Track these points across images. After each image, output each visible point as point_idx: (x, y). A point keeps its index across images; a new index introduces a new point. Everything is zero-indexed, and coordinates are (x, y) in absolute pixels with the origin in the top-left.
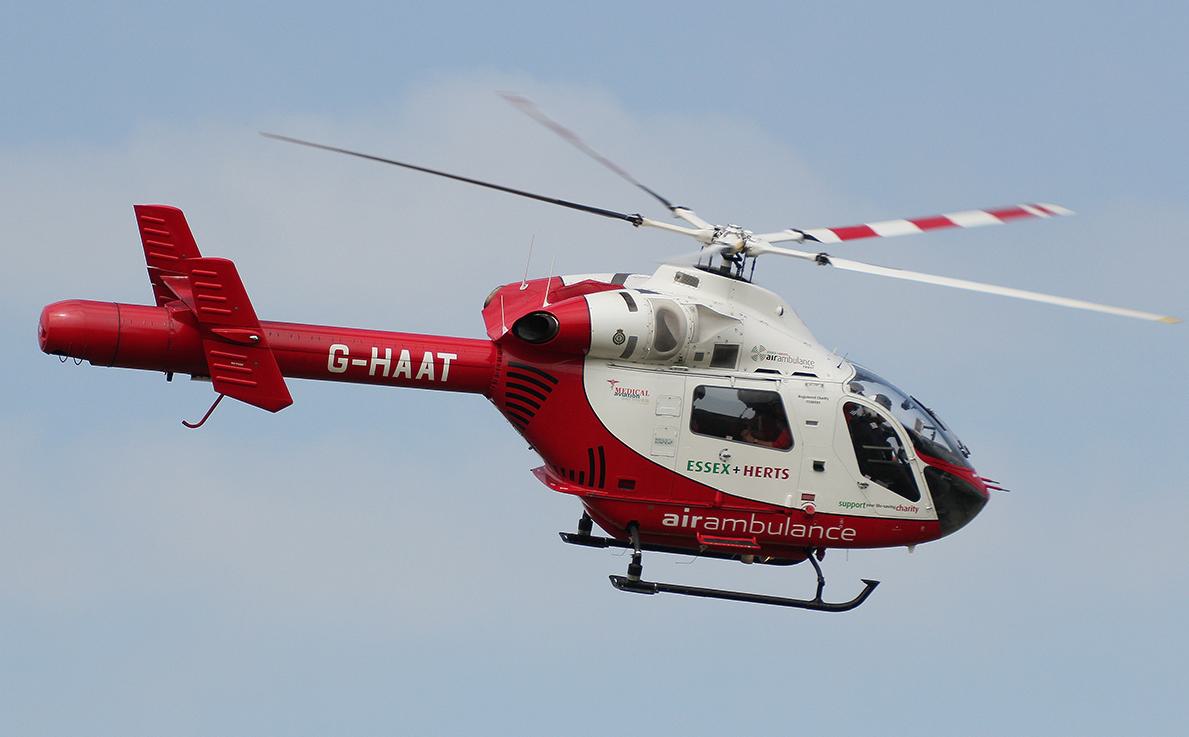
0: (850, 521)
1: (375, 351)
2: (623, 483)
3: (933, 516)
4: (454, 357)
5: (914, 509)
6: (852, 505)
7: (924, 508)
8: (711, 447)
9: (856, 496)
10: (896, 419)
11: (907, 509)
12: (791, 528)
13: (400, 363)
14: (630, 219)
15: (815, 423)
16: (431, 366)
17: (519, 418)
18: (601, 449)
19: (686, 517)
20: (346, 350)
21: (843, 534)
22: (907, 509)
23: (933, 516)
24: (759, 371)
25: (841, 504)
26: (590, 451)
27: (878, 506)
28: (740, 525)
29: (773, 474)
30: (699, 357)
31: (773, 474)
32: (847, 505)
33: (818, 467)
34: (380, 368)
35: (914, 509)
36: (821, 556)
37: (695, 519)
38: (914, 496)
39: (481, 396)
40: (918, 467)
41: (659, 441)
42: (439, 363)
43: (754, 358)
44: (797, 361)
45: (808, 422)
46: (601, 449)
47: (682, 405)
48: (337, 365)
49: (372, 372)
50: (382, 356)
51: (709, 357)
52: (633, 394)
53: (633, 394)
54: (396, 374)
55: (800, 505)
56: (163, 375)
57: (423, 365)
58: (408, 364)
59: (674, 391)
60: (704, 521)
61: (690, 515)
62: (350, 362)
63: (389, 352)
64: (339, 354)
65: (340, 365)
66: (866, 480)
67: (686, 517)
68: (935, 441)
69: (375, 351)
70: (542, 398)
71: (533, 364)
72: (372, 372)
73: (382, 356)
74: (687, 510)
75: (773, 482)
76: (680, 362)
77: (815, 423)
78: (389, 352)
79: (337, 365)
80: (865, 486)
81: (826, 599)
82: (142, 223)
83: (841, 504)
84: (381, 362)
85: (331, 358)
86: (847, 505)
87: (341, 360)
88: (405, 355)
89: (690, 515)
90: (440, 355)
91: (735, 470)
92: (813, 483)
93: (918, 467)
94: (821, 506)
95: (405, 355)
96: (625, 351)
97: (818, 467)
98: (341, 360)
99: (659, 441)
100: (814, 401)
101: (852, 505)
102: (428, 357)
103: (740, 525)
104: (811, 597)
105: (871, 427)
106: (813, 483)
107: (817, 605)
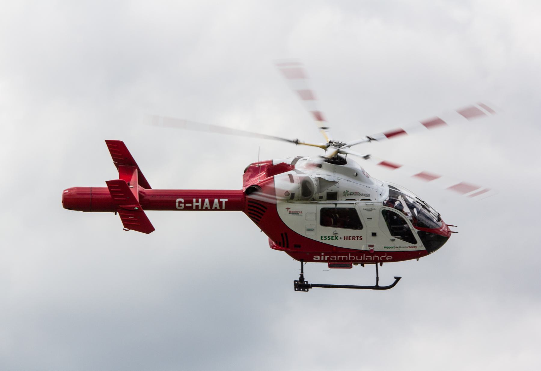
0: (389, 253)
1: (194, 200)
2: (296, 246)
3: (424, 248)
4: (227, 200)
5: (415, 247)
6: (389, 248)
7: (420, 246)
8: (329, 231)
9: (391, 244)
10: (407, 214)
11: (412, 247)
12: (366, 257)
13: (205, 204)
14: (293, 142)
15: (371, 219)
16: (218, 204)
17: (256, 219)
18: (286, 234)
19: (322, 257)
20: (182, 200)
21: (387, 258)
22: (412, 247)
23: (424, 248)
24: (347, 200)
25: (385, 248)
26: (282, 234)
27: (400, 247)
28: (345, 258)
29: (356, 239)
30: (321, 198)
31: (356, 239)
32: (387, 248)
33: (374, 234)
34: (197, 206)
35: (415, 247)
36: (381, 265)
37: (326, 257)
38: (415, 242)
39: (242, 212)
40: (415, 232)
41: (308, 230)
42: (220, 203)
43: (345, 195)
44: (363, 195)
45: (368, 219)
46: (286, 234)
47: (316, 214)
48: (179, 206)
49: (194, 208)
50: (197, 201)
51: (325, 197)
52: (296, 213)
53: (296, 213)
54: (204, 208)
55: (368, 249)
56: (114, 213)
57: (214, 204)
58: (208, 204)
59: (312, 210)
60: (330, 257)
61: (324, 256)
62: (185, 205)
63: (200, 200)
64: (180, 202)
65: (181, 206)
66: (393, 238)
67: (322, 257)
68: (375, 265)
69: (194, 200)
70: (264, 211)
71: (254, 203)
72: (194, 208)
73: (197, 201)
74: (323, 254)
75: (356, 241)
76: (314, 200)
77: (371, 219)
78: (200, 200)
79: (179, 206)
80: (394, 240)
81: (380, 285)
82: (109, 147)
83: (385, 248)
84: (197, 204)
85: (177, 204)
86: (387, 248)
87: (181, 205)
88: (207, 200)
89: (324, 256)
90: (221, 200)
91: (341, 238)
92: (373, 241)
93: (415, 232)
94: (377, 248)
95: (207, 200)
96: (291, 197)
97: (374, 234)
98: (181, 205)
99: (308, 230)
100: (370, 210)
101: (389, 248)
102: (216, 200)
103: (345, 258)
104: (374, 284)
105: (393, 218)
106: (373, 241)
107: (377, 287)
